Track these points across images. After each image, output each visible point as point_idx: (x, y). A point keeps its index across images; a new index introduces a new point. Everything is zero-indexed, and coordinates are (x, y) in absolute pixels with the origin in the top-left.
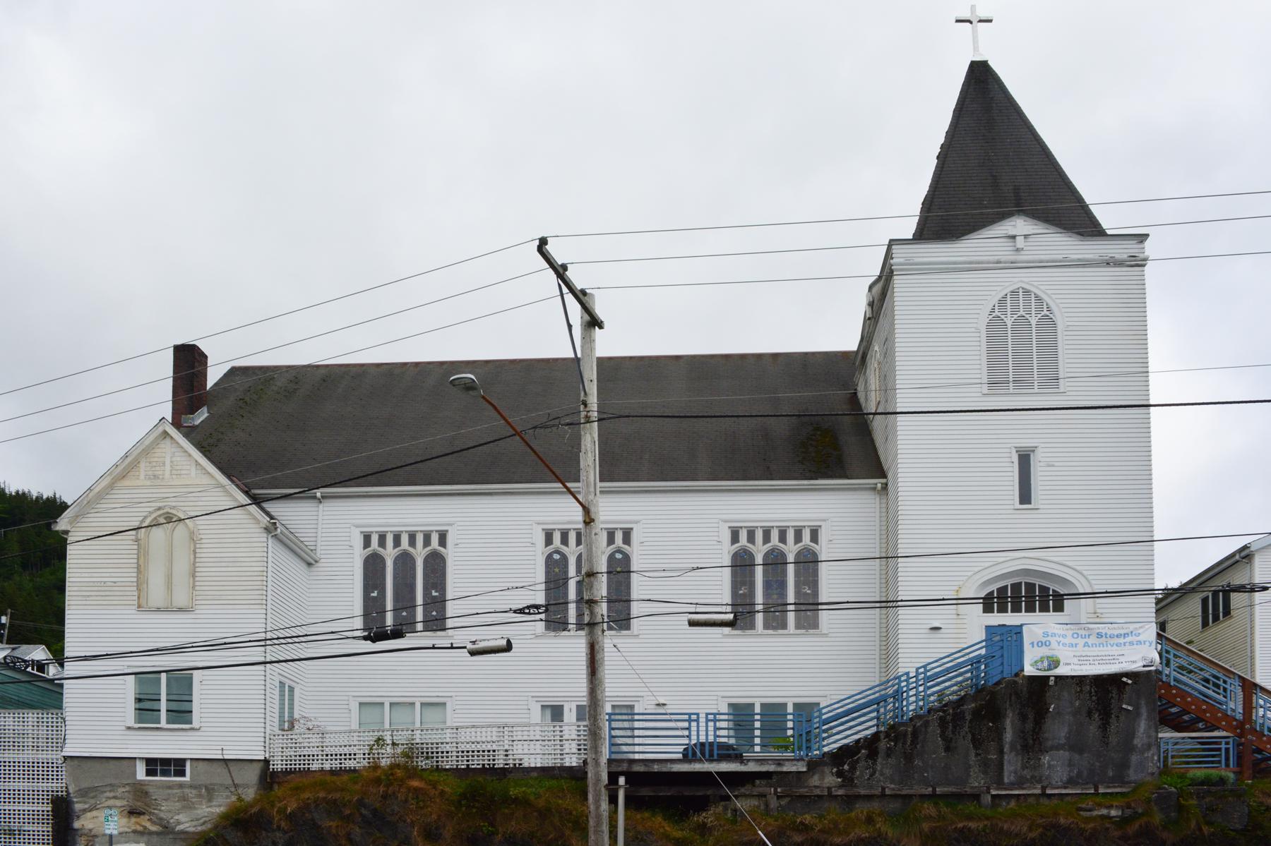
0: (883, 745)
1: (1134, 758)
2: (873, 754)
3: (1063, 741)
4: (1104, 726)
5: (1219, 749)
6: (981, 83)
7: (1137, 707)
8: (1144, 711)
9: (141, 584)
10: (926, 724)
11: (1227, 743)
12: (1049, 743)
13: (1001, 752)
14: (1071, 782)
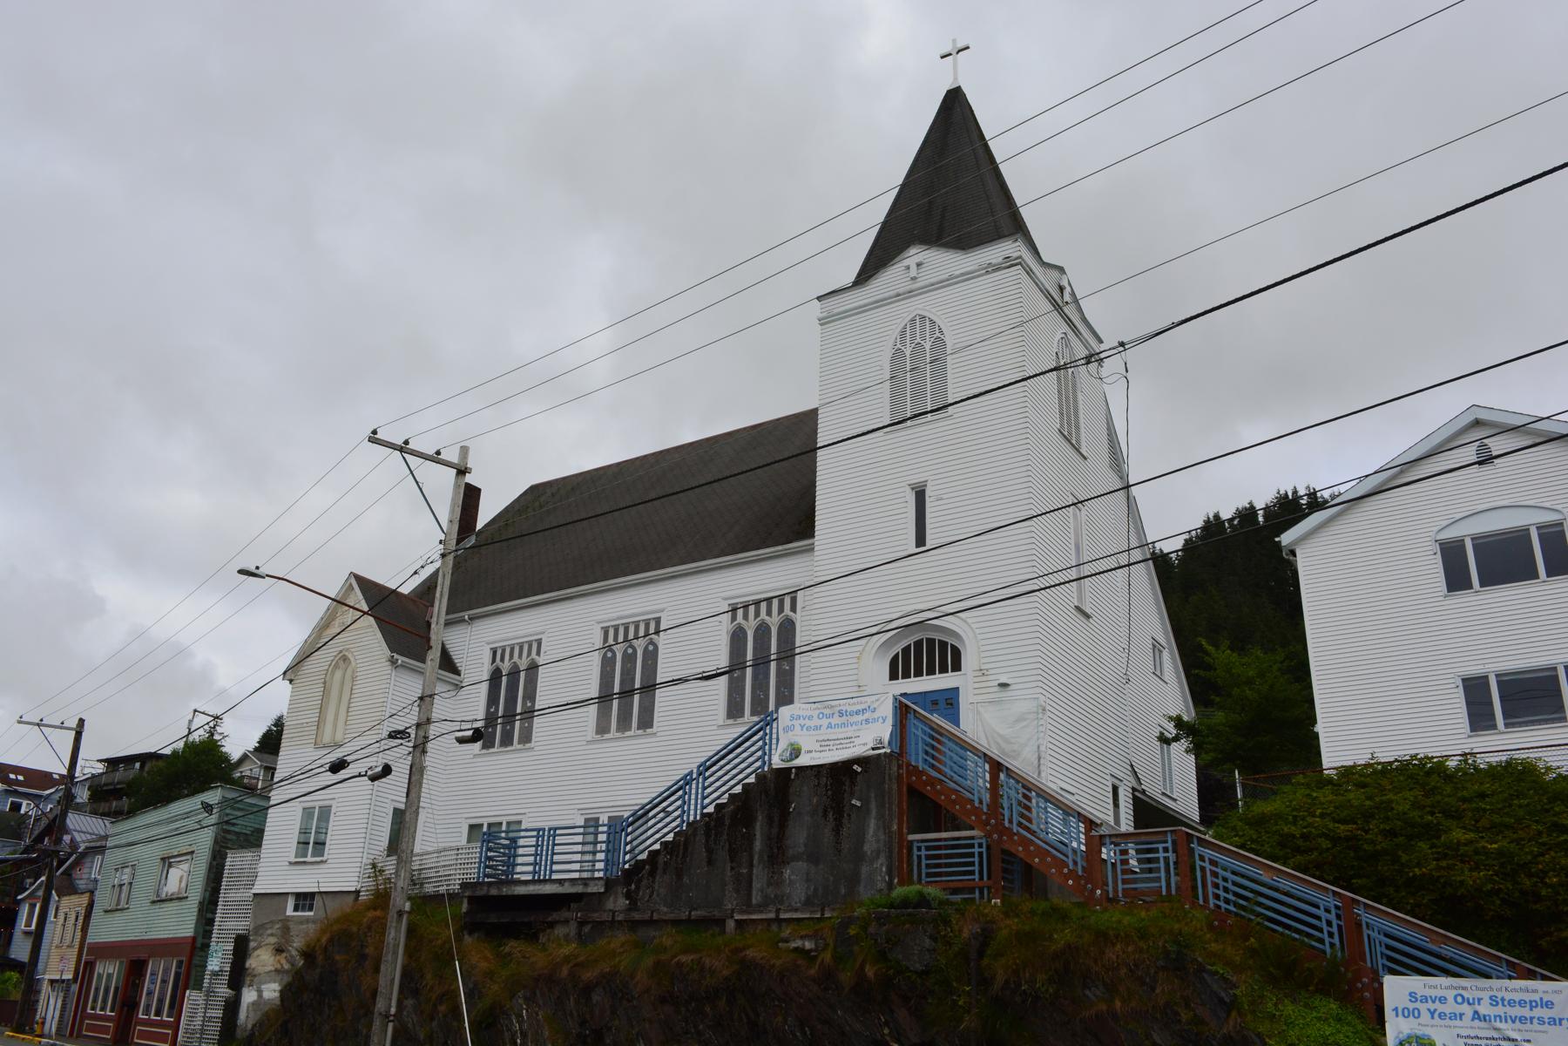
0: (661, 859)
1: (864, 869)
2: (652, 873)
3: (801, 849)
4: (837, 830)
5: (972, 855)
6: (955, 107)
7: (866, 802)
8: (873, 806)
9: (320, 724)
10: (695, 834)
11: (1166, 850)
12: (791, 852)
13: (751, 865)
14: (808, 903)
